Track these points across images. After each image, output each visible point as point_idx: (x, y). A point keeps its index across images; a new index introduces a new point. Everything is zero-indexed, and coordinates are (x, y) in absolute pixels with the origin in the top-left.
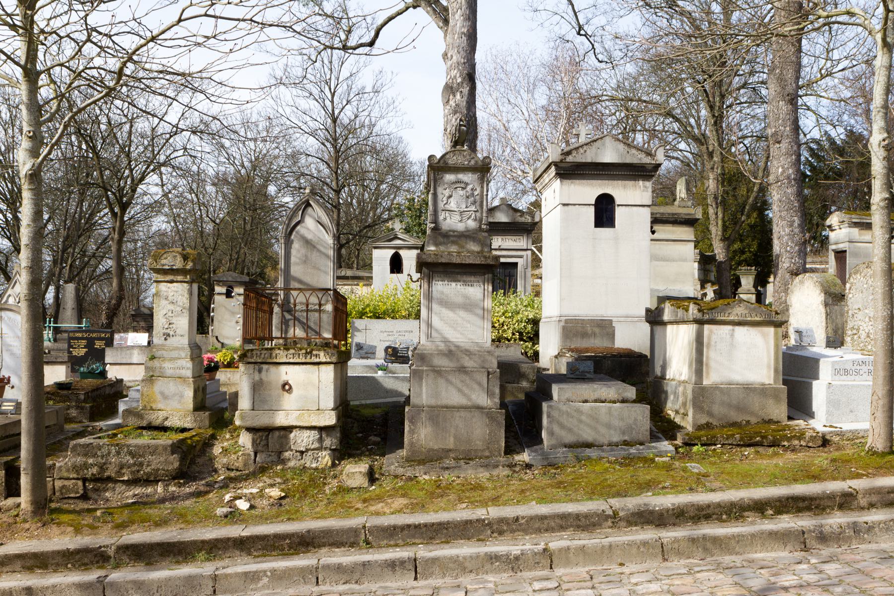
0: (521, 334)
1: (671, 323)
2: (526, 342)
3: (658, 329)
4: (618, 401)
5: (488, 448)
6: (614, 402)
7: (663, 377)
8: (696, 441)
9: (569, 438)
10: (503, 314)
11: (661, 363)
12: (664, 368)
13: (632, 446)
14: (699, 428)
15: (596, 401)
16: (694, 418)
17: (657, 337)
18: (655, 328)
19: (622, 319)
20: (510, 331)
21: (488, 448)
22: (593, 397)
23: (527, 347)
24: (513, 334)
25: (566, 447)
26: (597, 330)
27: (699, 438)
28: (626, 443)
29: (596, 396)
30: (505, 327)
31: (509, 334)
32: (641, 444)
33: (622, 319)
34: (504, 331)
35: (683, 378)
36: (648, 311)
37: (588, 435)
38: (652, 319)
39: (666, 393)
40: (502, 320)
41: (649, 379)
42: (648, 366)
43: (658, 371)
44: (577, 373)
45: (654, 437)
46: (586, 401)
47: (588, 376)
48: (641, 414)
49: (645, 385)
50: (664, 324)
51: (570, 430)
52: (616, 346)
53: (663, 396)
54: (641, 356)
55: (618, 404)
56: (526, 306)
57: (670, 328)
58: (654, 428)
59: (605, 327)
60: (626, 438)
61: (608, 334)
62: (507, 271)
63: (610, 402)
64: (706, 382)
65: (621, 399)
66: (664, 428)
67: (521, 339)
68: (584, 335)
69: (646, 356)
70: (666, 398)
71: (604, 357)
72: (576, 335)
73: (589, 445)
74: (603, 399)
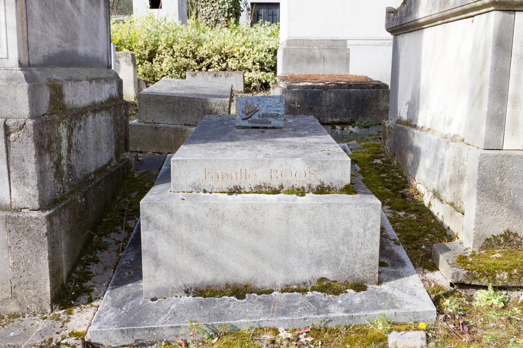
0: (261, 64)
1: (432, 22)
2: (267, 72)
3: (407, 40)
4: (311, 189)
5: (14, 296)
6: (301, 192)
7: (411, 124)
8: (484, 281)
9: (205, 275)
10: (244, 44)
11: (409, 98)
12: (414, 106)
13: (337, 292)
14: (489, 244)
15: (259, 190)
16: (478, 223)
17: (402, 54)
18: (400, 38)
19: (362, 42)
20: (250, 62)
21: (14, 296)
22: (253, 182)
23: (268, 77)
24: (254, 64)
25: (187, 292)
26: (327, 53)
27: (491, 274)
28: (326, 287)
29: (261, 176)
30: (246, 57)
31: (249, 64)
32: (359, 287)
33: (362, 42)
34: (244, 60)
35: (452, 130)
36: (390, 12)
37: (240, 269)
38: (396, 24)
39: (417, 152)
40: (242, 50)
41: (389, 123)
42: (388, 100)
43: (403, 112)
44: (255, 117)
45: (389, 264)
46: (236, 191)
47: (275, 122)
48: (366, 215)
49: (381, 129)
50: (416, 27)
51: (198, 255)
52: (350, 74)
53: (410, 157)
54: (379, 86)
55: (309, 197)
56: (269, 36)
57: (428, 33)
58: (389, 228)
59: (338, 49)
60: (326, 273)
61: (340, 58)
62: (271, 11)
63: (291, 191)
64: (510, 143)
65: (315, 184)
66: (414, 237)
67: (262, 70)
68: (311, 59)
69: (386, 86)
70: (416, 163)
71: (326, 88)
72: (300, 59)
73: (240, 292)
74: (275, 184)
